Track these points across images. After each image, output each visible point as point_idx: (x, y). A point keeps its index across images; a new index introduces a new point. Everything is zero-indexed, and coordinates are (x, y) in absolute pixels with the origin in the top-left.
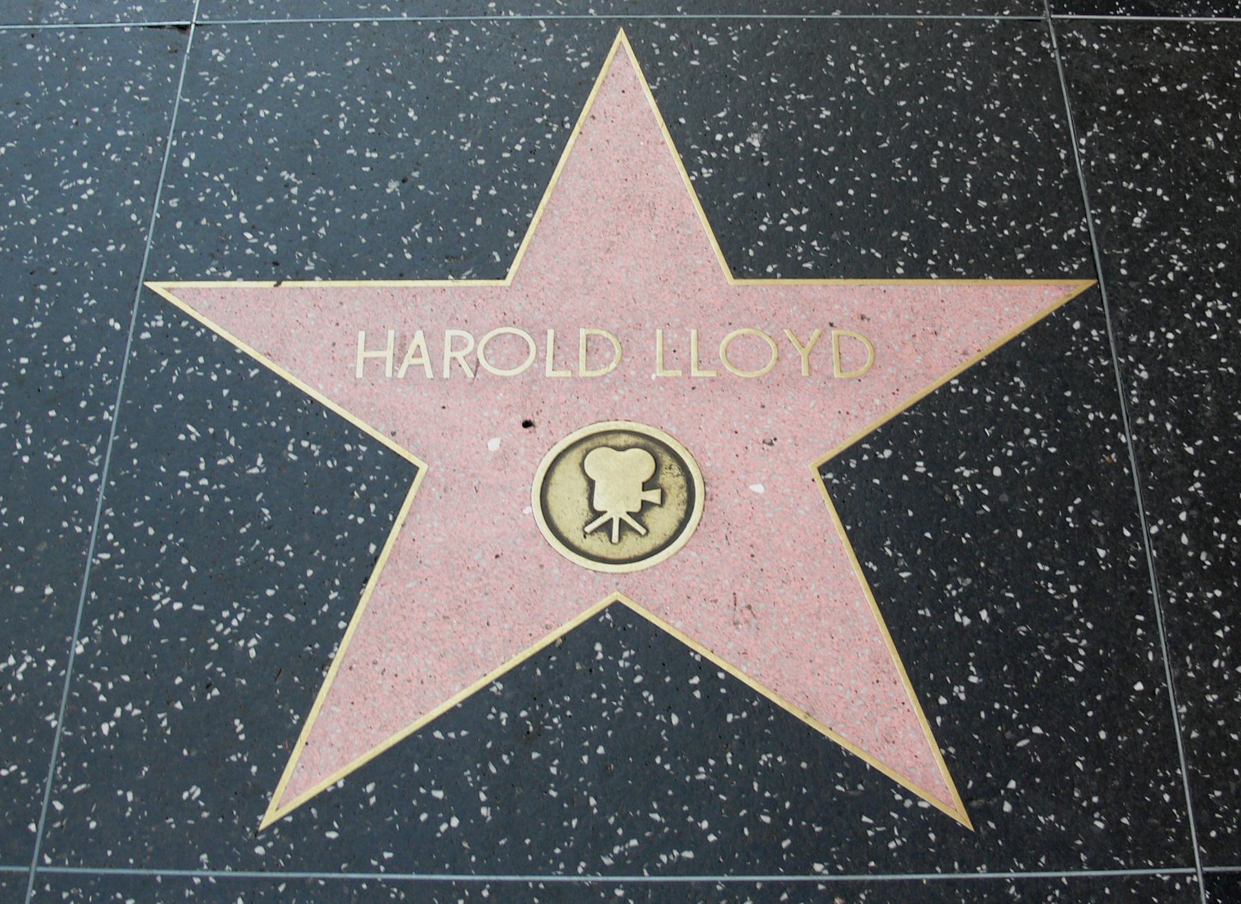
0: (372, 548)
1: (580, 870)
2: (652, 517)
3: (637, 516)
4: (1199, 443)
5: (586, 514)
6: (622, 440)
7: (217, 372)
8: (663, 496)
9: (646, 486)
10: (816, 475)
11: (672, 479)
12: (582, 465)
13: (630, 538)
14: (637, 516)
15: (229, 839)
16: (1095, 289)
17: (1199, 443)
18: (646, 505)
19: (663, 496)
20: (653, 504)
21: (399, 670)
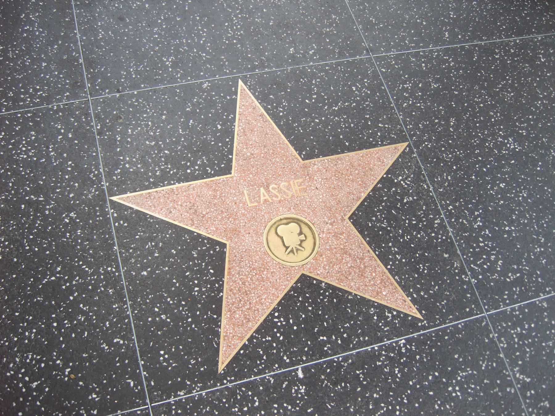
0: (195, 234)
1: (4, 111)
2: (304, 244)
3: (300, 245)
4: (149, 269)
5: (285, 249)
6: (285, 221)
7: (536, 335)
8: (306, 237)
9: (301, 233)
10: (348, 221)
11: (306, 230)
12: (276, 233)
13: (291, 254)
14: (300, 245)
15: (211, 375)
16: (409, 144)
17: (149, 269)
18: (302, 241)
19: (306, 237)
20: (304, 240)
21: (243, 315)
